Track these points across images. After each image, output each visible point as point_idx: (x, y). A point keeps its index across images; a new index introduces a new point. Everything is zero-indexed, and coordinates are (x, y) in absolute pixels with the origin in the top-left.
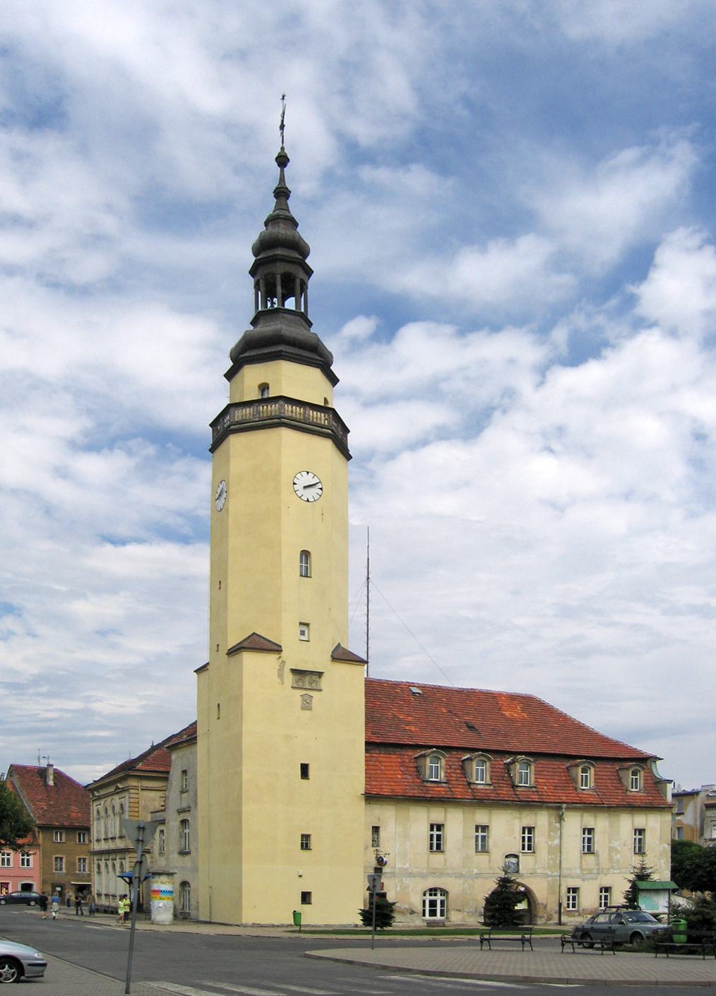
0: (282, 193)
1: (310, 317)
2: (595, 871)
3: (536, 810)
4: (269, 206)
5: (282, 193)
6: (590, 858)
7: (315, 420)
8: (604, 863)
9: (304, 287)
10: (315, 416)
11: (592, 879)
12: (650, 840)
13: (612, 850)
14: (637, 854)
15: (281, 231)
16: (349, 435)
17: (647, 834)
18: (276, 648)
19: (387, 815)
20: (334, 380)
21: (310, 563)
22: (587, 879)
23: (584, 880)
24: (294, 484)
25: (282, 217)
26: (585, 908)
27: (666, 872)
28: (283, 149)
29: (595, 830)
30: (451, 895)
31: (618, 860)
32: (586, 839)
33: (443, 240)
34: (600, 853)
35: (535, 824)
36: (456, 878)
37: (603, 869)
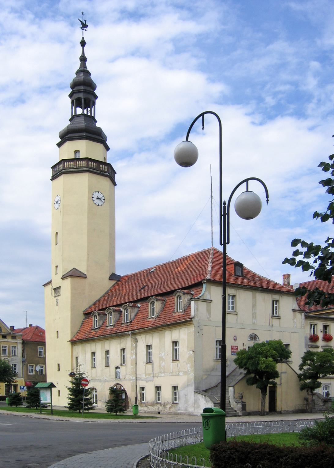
0: (83, 59)
1: (96, 118)
2: (152, 376)
3: (126, 337)
4: (77, 65)
5: (83, 59)
6: (149, 366)
7: (102, 169)
8: (157, 370)
9: (94, 104)
10: (104, 168)
11: (150, 381)
12: (182, 348)
13: (161, 359)
14: (174, 361)
15: (81, 106)
16: (116, 175)
17: (180, 343)
18: (85, 276)
19: (79, 349)
20: (107, 148)
21: (316, 328)
22: (149, 381)
23: (147, 382)
24: (93, 197)
25: (84, 71)
26: (148, 401)
27: (191, 374)
28: (83, 38)
29: (290, 345)
30: (98, 390)
31: (164, 367)
32: (218, 348)
33: (326, 307)
34: (154, 362)
35: (126, 346)
36: (99, 382)
37: (156, 374)
